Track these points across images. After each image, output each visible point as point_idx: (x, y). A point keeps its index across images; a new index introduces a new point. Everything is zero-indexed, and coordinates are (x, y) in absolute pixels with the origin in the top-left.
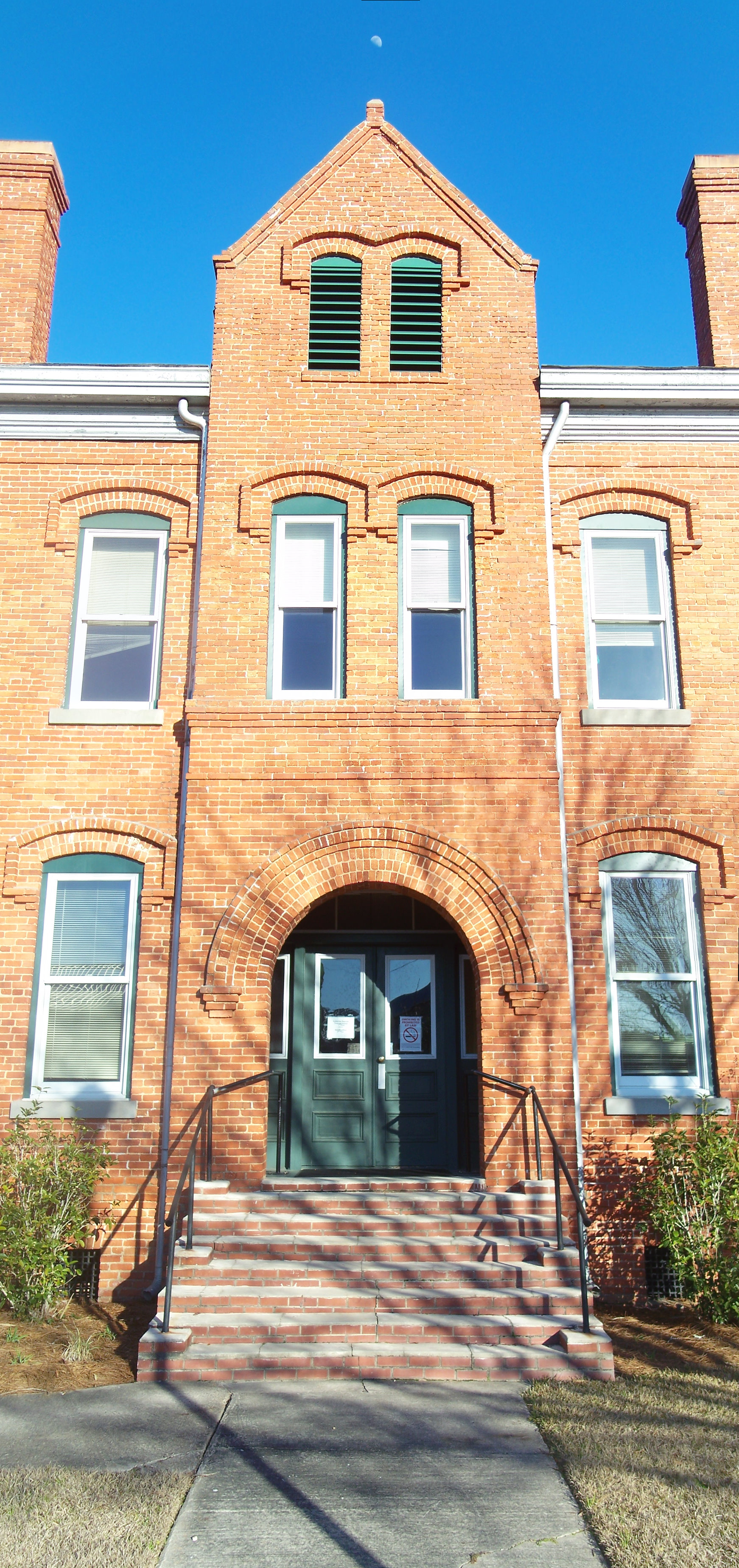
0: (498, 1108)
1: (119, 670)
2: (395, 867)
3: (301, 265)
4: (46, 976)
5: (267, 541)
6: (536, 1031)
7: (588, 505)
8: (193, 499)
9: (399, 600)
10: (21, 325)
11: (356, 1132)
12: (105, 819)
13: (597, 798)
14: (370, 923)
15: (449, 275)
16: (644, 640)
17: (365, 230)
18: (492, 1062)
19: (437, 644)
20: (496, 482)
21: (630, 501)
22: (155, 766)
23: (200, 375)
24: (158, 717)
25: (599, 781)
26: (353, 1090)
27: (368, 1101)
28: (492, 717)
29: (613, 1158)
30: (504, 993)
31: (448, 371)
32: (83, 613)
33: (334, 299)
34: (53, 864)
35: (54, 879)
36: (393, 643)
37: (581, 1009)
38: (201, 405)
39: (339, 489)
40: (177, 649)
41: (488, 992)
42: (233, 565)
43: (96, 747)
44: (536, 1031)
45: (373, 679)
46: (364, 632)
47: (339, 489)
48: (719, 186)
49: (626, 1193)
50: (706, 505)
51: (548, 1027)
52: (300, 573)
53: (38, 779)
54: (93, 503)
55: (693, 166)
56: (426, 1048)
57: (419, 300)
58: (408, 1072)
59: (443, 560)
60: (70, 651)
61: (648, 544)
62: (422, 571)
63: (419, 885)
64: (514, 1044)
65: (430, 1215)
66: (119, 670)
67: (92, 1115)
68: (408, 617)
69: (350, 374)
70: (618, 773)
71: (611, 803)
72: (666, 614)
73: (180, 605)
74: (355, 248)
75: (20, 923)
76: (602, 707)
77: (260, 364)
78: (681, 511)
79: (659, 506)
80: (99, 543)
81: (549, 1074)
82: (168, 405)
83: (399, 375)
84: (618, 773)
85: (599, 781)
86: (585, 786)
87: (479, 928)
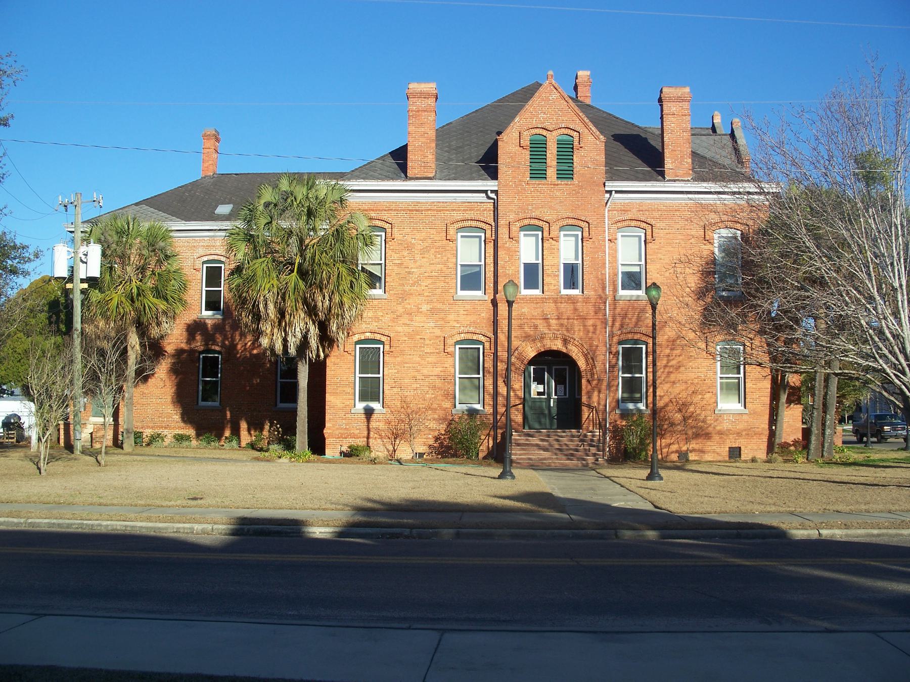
0: (585, 413)
1: (471, 280)
2: (558, 345)
3: (526, 142)
4: (458, 375)
5: (518, 241)
6: (596, 393)
7: (619, 225)
8: (493, 224)
9: (559, 262)
10: (430, 157)
11: (543, 420)
12: (472, 329)
13: (617, 324)
14: (554, 364)
15: (576, 143)
16: (637, 269)
17: (547, 125)
18: (584, 399)
19: (571, 275)
20: (590, 222)
21: (633, 223)
22: (486, 312)
23: (495, 183)
24: (486, 297)
25: (619, 319)
26: (541, 408)
27: (546, 412)
28: (586, 300)
29: (617, 425)
30: (588, 381)
31: (575, 181)
32: (459, 263)
33: (538, 149)
34: (457, 343)
35: (457, 347)
36: (558, 276)
37: (609, 386)
38: (496, 192)
39: (541, 223)
40: (490, 275)
41: (584, 381)
42: (508, 249)
43: (468, 307)
44: (596, 393)
45: (552, 287)
46: (549, 272)
47: (541, 223)
48: (671, 100)
49: (617, 433)
50: (658, 224)
51: (599, 392)
52: (527, 249)
53: (452, 317)
54: (461, 224)
55: (661, 92)
56: (565, 394)
57: (567, 150)
58: (559, 402)
59: (573, 243)
60: (456, 274)
61: (640, 237)
62: (567, 249)
63: (564, 350)
64: (590, 397)
65: (567, 437)
66: (471, 280)
67: (472, 413)
68: (562, 266)
69: (544, 181)
70: (625, 316)
71: (622, 326)
72: (643, 262)
73: (490, 260)
74: (544, 133)
75: (450, 360)
76: (623, 293)
77: (514, 177)
78: (650, 227)
79: (643, 225)
80: (462, 237)
81: (599, 404)
82: (485, 192)
83: (559, 182)
84: (625, 316)
85: (619, 319)
86: (614, 321)
87: (582, 363)
